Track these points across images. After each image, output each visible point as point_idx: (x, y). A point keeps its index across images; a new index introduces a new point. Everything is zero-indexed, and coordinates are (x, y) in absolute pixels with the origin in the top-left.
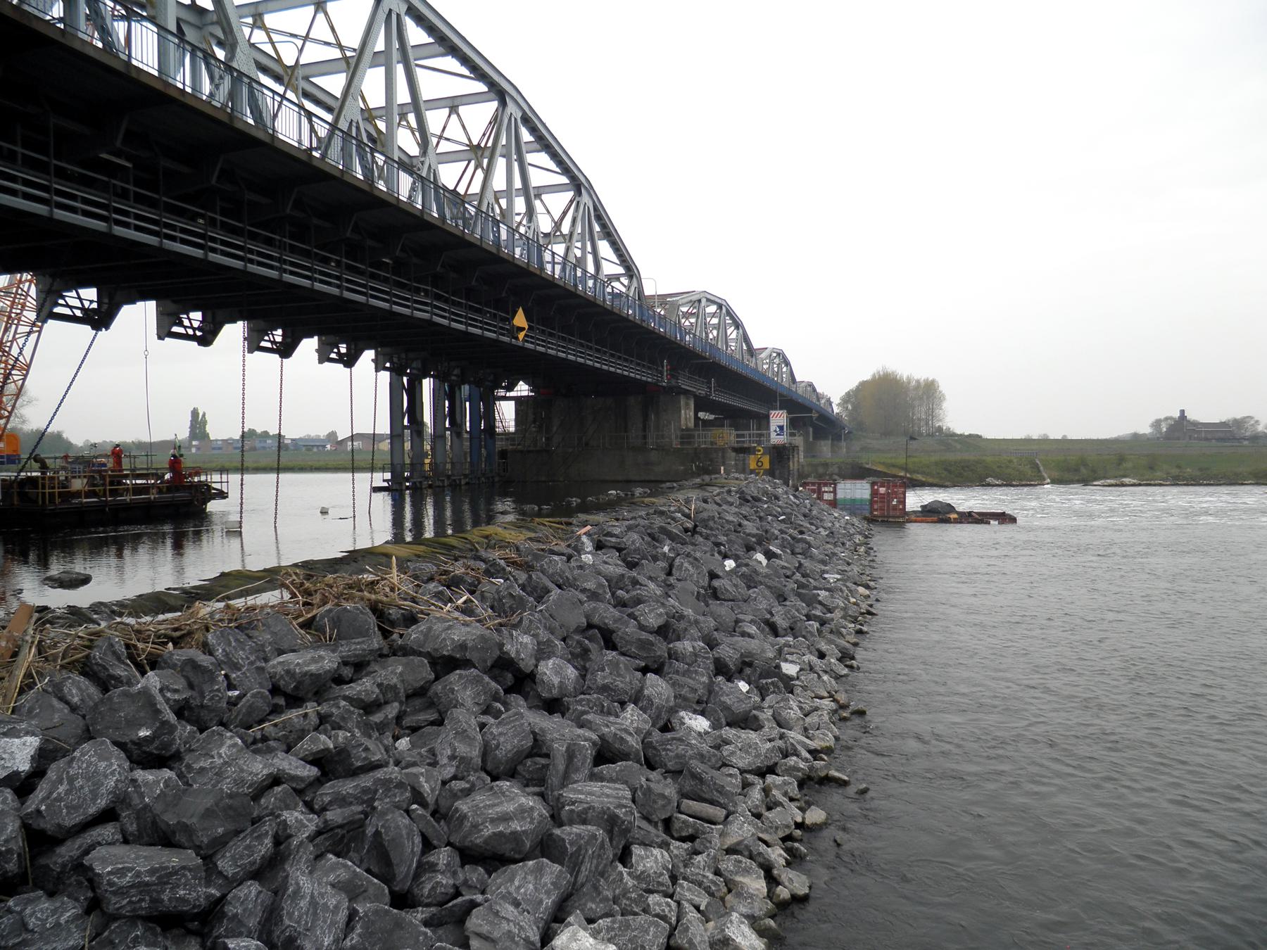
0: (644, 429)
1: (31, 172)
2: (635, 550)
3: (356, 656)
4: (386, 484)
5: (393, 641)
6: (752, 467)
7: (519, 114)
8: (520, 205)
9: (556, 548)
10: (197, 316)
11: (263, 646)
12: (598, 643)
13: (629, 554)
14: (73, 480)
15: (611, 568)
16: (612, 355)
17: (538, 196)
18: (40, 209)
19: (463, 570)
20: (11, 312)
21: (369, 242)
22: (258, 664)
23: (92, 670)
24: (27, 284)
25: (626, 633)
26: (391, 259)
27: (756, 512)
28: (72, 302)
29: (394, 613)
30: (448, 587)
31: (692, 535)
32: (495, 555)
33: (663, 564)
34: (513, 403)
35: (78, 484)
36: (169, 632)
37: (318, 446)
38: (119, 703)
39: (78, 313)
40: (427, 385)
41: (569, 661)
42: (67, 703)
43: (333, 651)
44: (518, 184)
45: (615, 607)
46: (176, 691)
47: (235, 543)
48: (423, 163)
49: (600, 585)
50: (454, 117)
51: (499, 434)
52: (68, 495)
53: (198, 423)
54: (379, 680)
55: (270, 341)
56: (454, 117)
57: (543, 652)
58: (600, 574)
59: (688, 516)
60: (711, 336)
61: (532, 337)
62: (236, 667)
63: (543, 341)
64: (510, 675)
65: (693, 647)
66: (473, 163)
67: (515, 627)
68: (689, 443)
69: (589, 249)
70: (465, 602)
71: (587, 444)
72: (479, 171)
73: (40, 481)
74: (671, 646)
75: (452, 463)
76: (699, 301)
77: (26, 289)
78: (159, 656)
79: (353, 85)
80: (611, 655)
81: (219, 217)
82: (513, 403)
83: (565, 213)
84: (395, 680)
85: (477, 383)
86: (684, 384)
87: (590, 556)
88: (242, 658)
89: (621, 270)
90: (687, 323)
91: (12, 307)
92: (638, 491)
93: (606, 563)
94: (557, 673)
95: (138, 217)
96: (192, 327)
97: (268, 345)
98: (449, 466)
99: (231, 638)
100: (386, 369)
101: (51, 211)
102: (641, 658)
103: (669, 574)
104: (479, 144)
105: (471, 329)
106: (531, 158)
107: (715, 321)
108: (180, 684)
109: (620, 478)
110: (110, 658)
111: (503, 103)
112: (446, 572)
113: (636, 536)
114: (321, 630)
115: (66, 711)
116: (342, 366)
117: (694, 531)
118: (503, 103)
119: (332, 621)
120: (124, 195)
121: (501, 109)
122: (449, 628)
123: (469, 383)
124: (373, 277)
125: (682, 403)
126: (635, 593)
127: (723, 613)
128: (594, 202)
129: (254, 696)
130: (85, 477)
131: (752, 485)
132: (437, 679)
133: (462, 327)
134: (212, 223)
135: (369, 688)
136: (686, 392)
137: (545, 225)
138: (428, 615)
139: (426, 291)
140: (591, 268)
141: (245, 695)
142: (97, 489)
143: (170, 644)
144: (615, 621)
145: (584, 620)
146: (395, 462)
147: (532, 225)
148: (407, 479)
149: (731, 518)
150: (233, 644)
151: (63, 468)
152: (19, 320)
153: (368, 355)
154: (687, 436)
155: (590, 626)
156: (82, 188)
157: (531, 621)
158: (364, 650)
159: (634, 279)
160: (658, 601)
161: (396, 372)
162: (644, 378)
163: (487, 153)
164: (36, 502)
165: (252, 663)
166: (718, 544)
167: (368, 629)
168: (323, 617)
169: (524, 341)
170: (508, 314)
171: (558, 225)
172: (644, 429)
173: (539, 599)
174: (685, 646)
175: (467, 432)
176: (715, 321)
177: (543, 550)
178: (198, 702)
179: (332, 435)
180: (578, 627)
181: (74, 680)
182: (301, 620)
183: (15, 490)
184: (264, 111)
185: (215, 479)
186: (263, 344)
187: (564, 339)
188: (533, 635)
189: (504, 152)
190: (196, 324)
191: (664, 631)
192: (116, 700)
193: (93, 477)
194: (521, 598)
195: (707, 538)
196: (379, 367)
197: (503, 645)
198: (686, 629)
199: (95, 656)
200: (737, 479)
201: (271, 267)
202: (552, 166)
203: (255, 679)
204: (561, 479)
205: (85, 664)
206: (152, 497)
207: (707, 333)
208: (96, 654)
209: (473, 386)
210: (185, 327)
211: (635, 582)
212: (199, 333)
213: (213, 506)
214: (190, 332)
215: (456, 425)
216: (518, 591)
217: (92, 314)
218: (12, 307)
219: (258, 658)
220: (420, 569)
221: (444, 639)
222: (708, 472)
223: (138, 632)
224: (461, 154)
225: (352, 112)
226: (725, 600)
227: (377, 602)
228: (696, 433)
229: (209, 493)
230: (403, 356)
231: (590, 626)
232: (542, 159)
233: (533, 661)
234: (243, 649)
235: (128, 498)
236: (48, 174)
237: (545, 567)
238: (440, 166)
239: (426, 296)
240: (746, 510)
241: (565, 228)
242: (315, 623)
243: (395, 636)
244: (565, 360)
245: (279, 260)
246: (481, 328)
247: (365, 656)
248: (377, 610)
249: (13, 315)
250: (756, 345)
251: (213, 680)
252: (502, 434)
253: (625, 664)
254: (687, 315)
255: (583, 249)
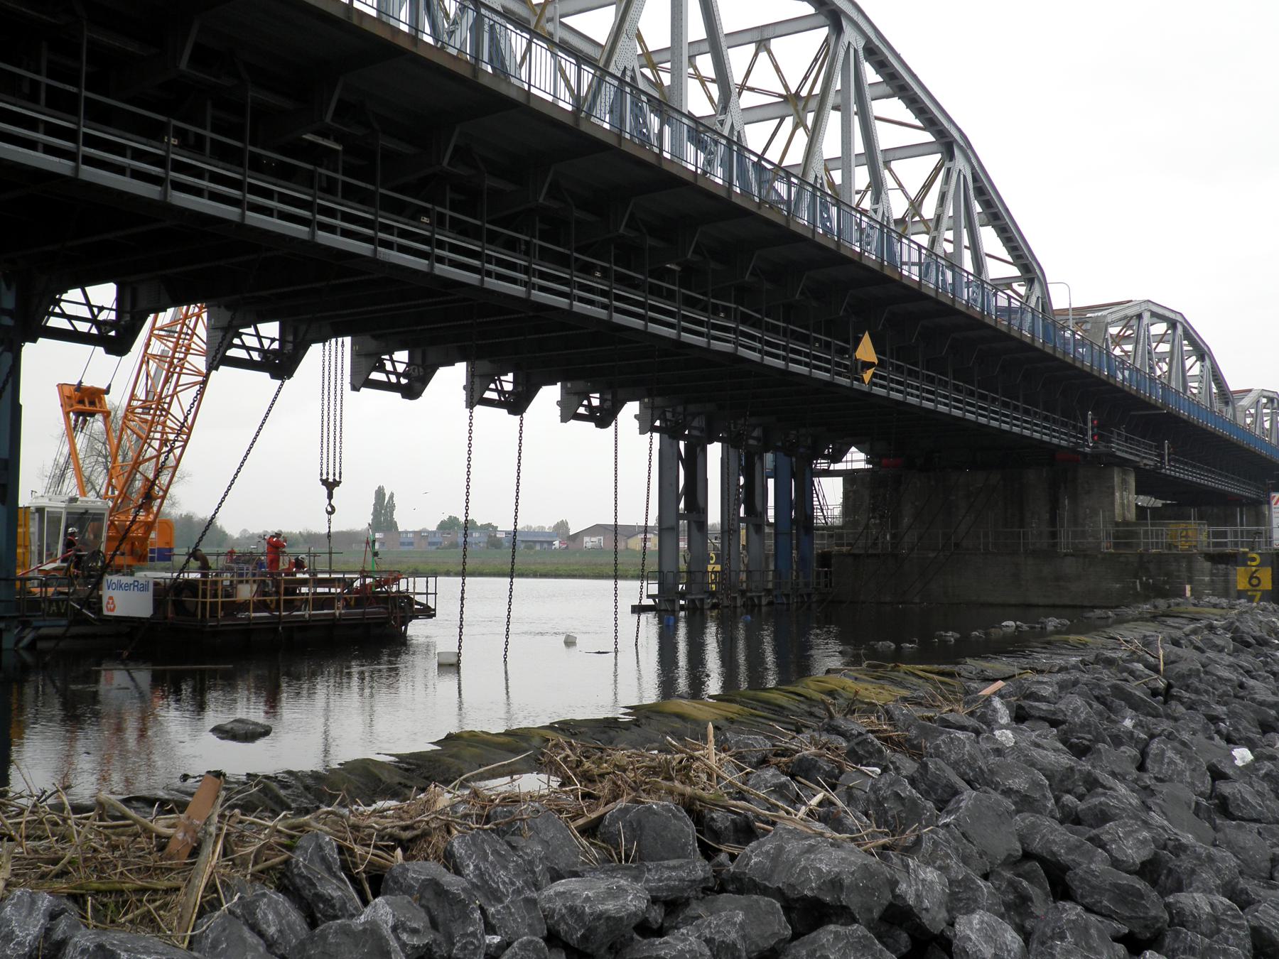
0: (1053, 521)
1: (221, 164)
2: (1082, 725)
3: (670, 889)
4: (650, 602)
5: (721, 865)
6: (1240, 588)
7: (860, 44)
8: (861, 177)
9: (951, 717)
10: (402, 356)
11: (531, 863)
12: (1041, 887)
13: (1071, 731)
14: (240, 586)
15: (1052, 756)
16: (1005, 405)
17: (887, 164)
18: (230, 212)
19: (813, 750)
20: (173, 357)
21: (650, 241)
22: (528, 894)
23: (294, 884)
24: (194, 319)
25: (1092, 872)
26: (678, 264)
27: (1266, 664)
28: (252, 342)
29: (720, 818)
30: (793, 777)
31: (1165, 702)
32: (857, 725)
33: (1130, 751)
34: (839, 481)
35: (246, 592)
36: (396, 831)
37: (541, 542)
38: (338, 945)
39: (256, 356)
40: (714, 452)
41: (1002, 916)
42: (261, 934)
43: (636, 879)
44: (859, 147)
45: (1061, 822)
46: (414, 931)
47: (449, 683)
48: (722, 123)
49: (1036, 784)
50: (763, 56)
51: (818, 529)
52: (235, 607)
53: (383, 507)
54: (707, 933)
55: (495, 390)
56: (763, 56)
57: (960, 899)
58: (1033, 765)
59: (1155, 669)
60: (1159, 372)
61: (882, 378)
62: (496, 896)
63: (899, 383)
64: (905, 936)
65: (1212, 905)
66: (789, 122)
67: (909, 850)
68: (1128, 545)
69: (966, 241)
70: (820, 804)
71: (957, 545)
72: (801, 131)
73: (201, 587)
74: (1171, 899)
75: (749, 572)
76: (1139, 316)
77: (192, 326)
78: (383, 868)
79: (628, 19)
80: (1072, 911)
81: (448, 212)
82: (839, 481)
83: (927, 187)
84: (733, 935)
85: (787, 450)
86: (1119, 448)
87: (1009, 733)
88: (504, 883)
89: (1014, 272)
90: (1117, 352)
91: (175, 352)
92: (1052, 623)
93: (1038, 745)
94: (989, 939)
95: (347, 217)
96: (395, 372)
97: (494, 396)
98: (743, 576)
99: (486, 847)
100: (654, 429)
101: (243, 215)
102: (1122, 919)
103: (1141, 767)
104: (797, 93)
105: (794, 367)
106: (880, 108)
107: (1164, 348)
108: (420, 922)
109: (1013, 601)
110: (318, 867)
111: (837, 29)
112: (785, 752)
113: (1079, 701)
114: (612, 840)
115: (261, 949)
116: (593, 424)
117: (1167, 694)
118: (837, 29)
119: (629, 825)
120: (329, 188)
121: (834, 38)
122: (811, 849)
123: (775, 450)
124: (655, 291)
125: (1117, 480)
126: (1095, 801)
127: (1250, 844)
128: (973, 168)
129: (524, 947)
130: (254, 581)
131: (1247, 616)
132: (796, 936)
133: (779, 363)
134: (440, 221)
135: (695, 947)
136: (1123, 464)
137: (898, 206)
138: (774, 824)
139: (726, 309)
140: (968, 264)
141: (509, 944)
142: (268, 599)
143: (399, 851)
144: (1070, 850)
145: (1018, 845)
146: (665, 570)
147: (880, 207)
148: (682, 595)
149: (1226, 674)
150: (491, 858)
151: (229, 569)
152: (182, 367)
153: (631, 409)
154: (1124, 534)
155: (1028, 856)
156: (282, 182)
157: (936, 844)
158: (682, 880)
159: (1036, 285)
160: (1136, 818)
161: (670, 433)
162: (1055, 441)
163: (813, 104)
164: (195, 615)
165: (518, 892)
166: (1214, 719)
167: (686, 844)
168: (615, 820)
169: (872, 384)
170: (847, 342)
171: (916, 205)
172: (1053, 521)
173: (942, 805)
174: (1197, 901)
175: (769, 524)
176: (1164, 348)
177: (930, 719)
178: (444, 951)
179: (562, 526)
180: (1010, 855)
181: (270, 898)
182: (581, 822)
183: (170, 598)
184: (507, 58)
185: (415, 586)
186: (488, 395)
187: (931, 380)
188: (940, 868)
189: (839, 100)
190: (401, 368)
191: (1149, 870)
192: (331, 939)
193: (264, 581)
194: (914, 802)
195: (1191, 706)
196: (646, 426)
197: (896, 883)
198: (1193, 872)
199: (297, 862)
200: (1215, 606)
201: (514, 281)
202: (909, 117)
203: (523, 918)
204: (917, 600)
205: (283, 874)
206: (337, 613)
207: (1152, 368)
208: (299, 858)
209: (780, 454)
210: (387, 373)
211: (1092, 783)
212: (404, 381)
213: (416, 629)
214: (393, 379)
215: (755, 512)
216: (908, 791)
217: (272, 357)
218: (175, 352)
219: (526, 882)
220: (747, 745)
221: (805, 868)
222: (1164, 595)
223: (355, 828)
224: (771, 108)
225: (626, 57)
226: (1242, 819)
227: (694, 798)
228: (1142, 530)
229: (411, 609)
230: (680, 409)
231: (1028, 856)
232: (894, 108)
233: (943, 915)
234: (505, 868)
235: (306, 613)
236: (241, 165)
237: (943, 748)
238: (747, 127)
239: (727, 318)
240: (1246, 660)
241: (929, 210)
242: (601, 829)
243: (723, 857)
244: (934, 412)
245: (526, 270)
246: (806, 365)
247: (684, 890)
248: (694, 809)
249: (175, 361)
250: (1233, 385)
251: (465, 917)
252: (823, 528)
253: (1098, 930)
254: (1119, 339)
255: (957, 242)
